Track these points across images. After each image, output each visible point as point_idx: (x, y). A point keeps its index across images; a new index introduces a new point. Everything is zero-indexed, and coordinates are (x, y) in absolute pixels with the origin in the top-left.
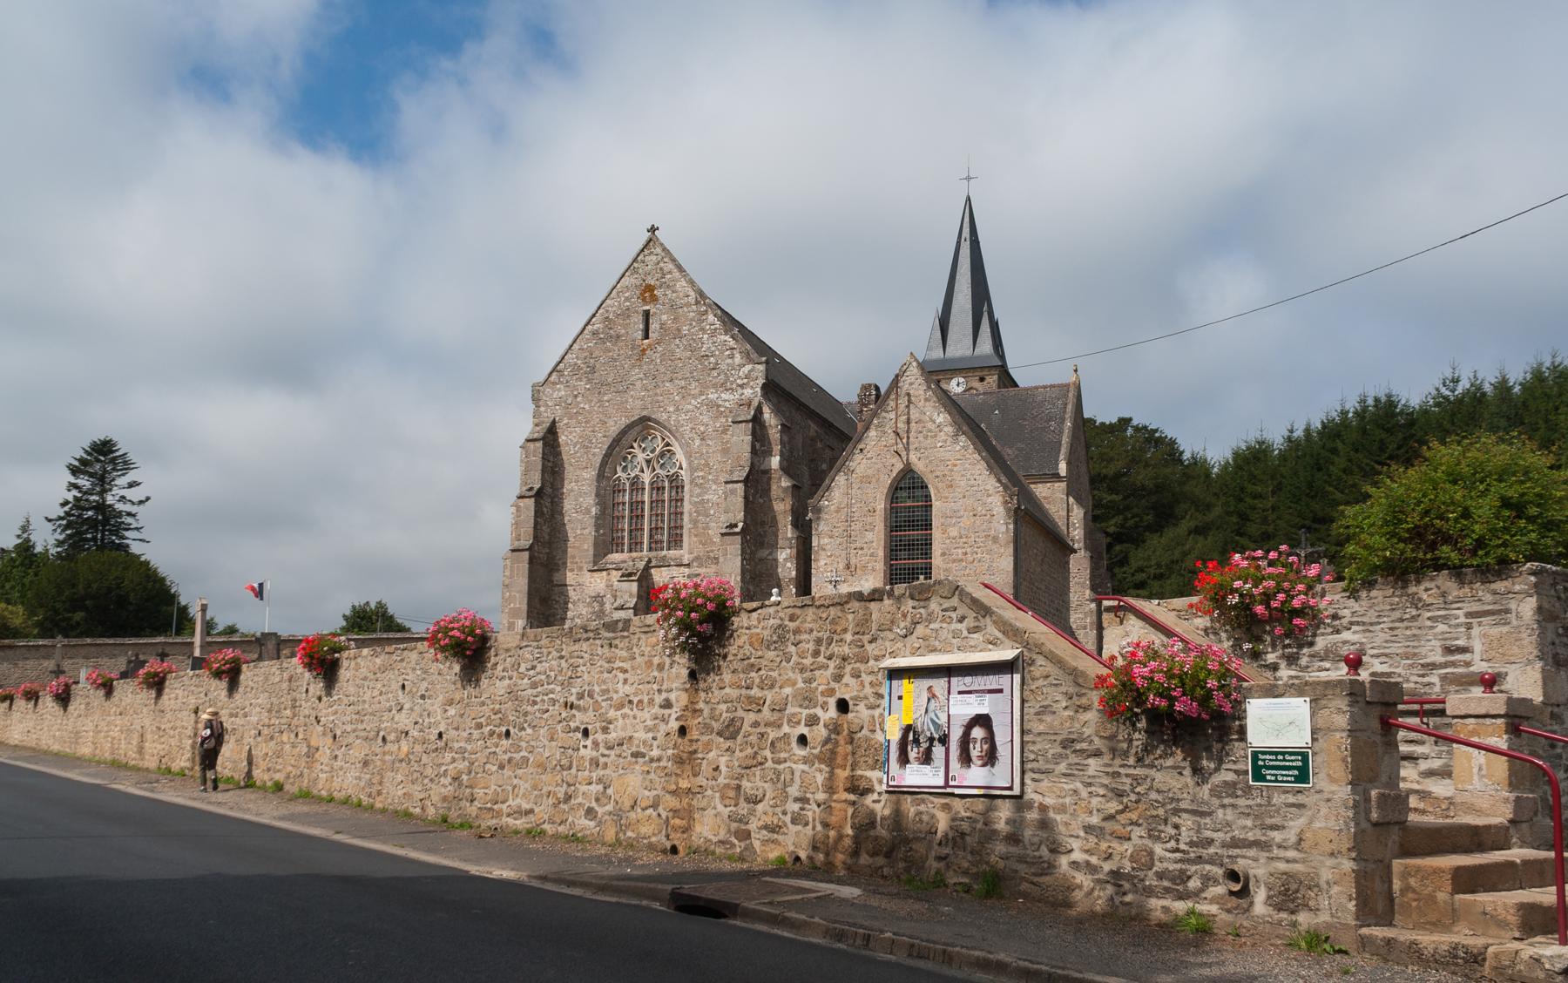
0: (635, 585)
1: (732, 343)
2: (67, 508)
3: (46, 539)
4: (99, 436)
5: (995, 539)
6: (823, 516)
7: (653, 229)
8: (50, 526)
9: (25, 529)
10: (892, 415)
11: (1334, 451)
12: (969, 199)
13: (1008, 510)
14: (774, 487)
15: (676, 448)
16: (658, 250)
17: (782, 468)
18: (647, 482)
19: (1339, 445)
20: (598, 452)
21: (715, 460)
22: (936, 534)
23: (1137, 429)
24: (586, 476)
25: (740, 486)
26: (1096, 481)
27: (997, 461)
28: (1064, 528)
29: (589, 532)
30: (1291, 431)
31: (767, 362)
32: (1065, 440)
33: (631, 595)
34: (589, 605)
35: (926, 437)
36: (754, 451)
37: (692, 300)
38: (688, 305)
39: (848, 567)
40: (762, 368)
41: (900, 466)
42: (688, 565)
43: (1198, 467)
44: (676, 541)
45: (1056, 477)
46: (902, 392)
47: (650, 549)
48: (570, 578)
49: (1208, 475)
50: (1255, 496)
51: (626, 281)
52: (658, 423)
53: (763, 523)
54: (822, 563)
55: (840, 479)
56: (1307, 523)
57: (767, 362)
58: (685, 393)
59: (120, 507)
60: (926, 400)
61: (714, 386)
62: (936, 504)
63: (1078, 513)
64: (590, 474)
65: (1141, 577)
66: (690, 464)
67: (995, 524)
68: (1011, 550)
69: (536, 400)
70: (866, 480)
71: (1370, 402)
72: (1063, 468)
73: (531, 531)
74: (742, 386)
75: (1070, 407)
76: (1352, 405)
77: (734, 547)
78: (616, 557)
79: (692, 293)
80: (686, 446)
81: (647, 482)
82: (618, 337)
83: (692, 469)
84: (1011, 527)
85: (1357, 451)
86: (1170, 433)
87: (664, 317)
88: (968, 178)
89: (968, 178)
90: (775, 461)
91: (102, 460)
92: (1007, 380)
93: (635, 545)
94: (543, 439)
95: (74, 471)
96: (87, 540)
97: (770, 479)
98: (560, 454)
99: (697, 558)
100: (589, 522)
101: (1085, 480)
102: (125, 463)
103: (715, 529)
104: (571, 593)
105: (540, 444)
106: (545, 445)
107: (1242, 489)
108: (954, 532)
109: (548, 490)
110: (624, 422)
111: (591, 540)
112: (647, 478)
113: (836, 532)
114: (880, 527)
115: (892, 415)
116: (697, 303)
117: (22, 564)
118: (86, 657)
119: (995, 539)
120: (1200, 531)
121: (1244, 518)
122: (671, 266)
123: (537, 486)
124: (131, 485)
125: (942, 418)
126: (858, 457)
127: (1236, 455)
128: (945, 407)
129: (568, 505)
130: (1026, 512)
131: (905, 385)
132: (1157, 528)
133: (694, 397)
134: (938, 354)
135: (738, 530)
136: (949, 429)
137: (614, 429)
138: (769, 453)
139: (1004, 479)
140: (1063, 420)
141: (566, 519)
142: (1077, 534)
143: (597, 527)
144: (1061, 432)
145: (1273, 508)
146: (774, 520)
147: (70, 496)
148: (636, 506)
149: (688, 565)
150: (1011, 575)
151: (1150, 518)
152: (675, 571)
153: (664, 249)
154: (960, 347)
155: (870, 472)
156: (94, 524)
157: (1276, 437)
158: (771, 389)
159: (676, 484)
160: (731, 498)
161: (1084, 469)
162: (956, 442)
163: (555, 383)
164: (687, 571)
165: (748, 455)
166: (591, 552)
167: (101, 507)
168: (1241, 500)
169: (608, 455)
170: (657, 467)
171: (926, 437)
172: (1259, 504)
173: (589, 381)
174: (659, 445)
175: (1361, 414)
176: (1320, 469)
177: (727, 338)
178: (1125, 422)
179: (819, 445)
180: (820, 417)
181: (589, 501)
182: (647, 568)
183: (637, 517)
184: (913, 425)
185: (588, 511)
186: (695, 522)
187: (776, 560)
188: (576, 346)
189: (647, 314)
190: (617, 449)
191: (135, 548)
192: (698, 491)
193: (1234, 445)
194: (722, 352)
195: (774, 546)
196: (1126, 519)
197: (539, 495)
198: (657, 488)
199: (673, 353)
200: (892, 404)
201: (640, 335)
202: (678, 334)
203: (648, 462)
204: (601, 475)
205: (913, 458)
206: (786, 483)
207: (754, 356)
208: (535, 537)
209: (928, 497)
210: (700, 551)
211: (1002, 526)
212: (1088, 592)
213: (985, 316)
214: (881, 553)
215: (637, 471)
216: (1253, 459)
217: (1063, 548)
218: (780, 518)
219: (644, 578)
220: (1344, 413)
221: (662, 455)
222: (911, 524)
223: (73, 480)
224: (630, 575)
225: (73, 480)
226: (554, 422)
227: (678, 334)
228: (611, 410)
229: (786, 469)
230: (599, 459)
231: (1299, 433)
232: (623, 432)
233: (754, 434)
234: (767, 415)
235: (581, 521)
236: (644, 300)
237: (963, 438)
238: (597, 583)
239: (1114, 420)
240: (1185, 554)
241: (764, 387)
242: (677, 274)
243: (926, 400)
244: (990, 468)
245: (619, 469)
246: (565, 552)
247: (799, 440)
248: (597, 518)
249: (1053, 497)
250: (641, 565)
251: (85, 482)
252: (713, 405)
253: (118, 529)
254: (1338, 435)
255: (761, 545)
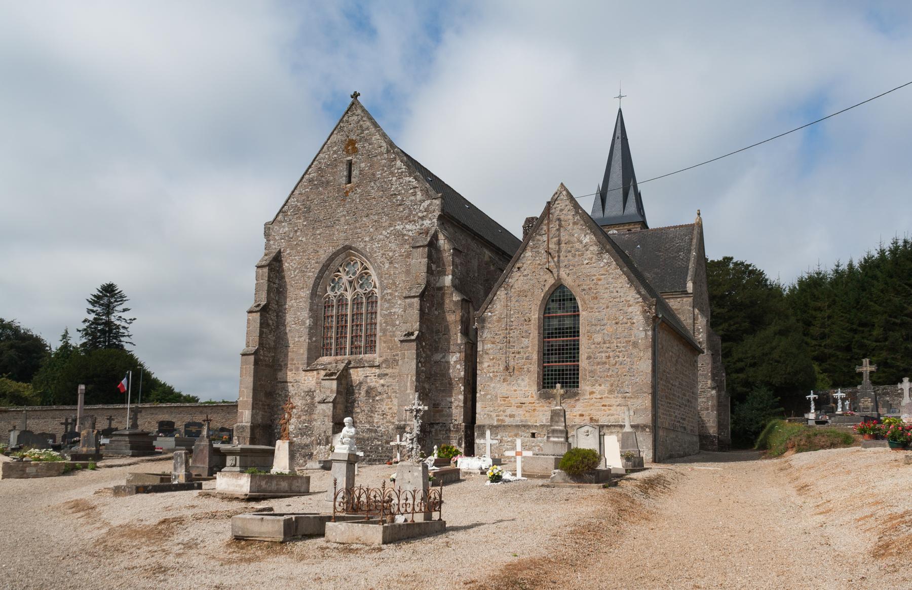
0: (335, 383)
1: (415, 183)
2: (87, 324)
3: (77, 340)
4: (106, 282)
5: (635, 345)
6: (487, 325)
7: (355, 95)
8: (80, 334)
9: (65, 336)
10: (545, 238)
11: (875, 277)
12: (620, 111)
13: (647, 319)
14: (447, 301)
15: (371, 271)
16: (359, 111)
17: (454, 286)
18: (349, 299)
19: (879, 273)
20: (312, 275)
21: (401, 279)
22: (583, 340)
23: (736, 264)
24: (303, 294)
25: (417, 300)
26: (712, 298)
27: (636, 274)
28: (692, 332)
29: (305, 339)
30: (838, 266)
31: (442, 197)
32: (691, 265)
33: (332, 391)
34: (304, 398)
35: (574, 256)
36: (429, 271)
37: (384, 150)
38: (381, 154)
39: (507, 368)
40: (438, 202)
41: (551, 281)
42: (378, 366)
43: (774, 292)
44: (371, 347)
45: (685, 292)
46: (553, 217)
47: (352, 353)
48: (290, 376)
49: (781, 295)
50: (816, 309)
51: (335, 138)
52: (357, 250)
53: (438, 332)
54: (486, 365)
55: (501, 293)
56: (855, 327)
57: (442, 197)
58: (378, 226)
59: (118, 323)
60: (574, 223)
61: (401, 219)
62: (583, 314)
63: (702, 322)
64: (305, 293)
65: (740, 365)
66: (381, 283)
67: (635, 331)
68: (649, 354)
69: (267, 235)
70: (523, 293)
71: (901, 243)
72: (690, 286)
73: (257, 339)
74: (422, 218)
75: (695, 241)
76: (887, 245)
77: (409, 355)
78: (325, 359)
79: (384, 144)
80: (378, 268)
81: (349, 299)
82: (328, 182)
83: (383, 288)
84: (650, 333)
85: (891, 277)
86: (759, 267)
87: (363, 165)
88: (620, 97)
89: (620, 97)
90: (448, 280)
91: (108, 296)
92: (644, 225)
93: (340, 350)
94: (269, 265)
95: (93, 303)
96: (100, 342)
97: (444, 294)
98: (283, 277)
99: (386, 361)
100: (305, 331)
101: (706, 296)
102: (121, 297)
103: (399, 335)
104: (290, 388)
105: (266, 270)
106: (270, 270)
107: (806, 305)
108: (598, 338)
109: (274, 306)
110: (331, 250)
111: (306, 346)
112: (349, 296)
113: (498, 339)
114: (534, 333)
115: (545, 238)
116: (388, 152)
117: (63, 356)
118: (53, 418)
119: (635, 345)
120: (783, 333)
121: (808, 324)
122: (368, 123)
123: (263, 303)
124: (125, 310)
125: (588, 238)
126: (516, 274)
127: (801, 282)
128: (590, 228)
129: (289, 318)
130: (664, 321)
131: (556, 212)
132: (752, 331)
133: (385, 229)
134: (599, 215)
135: (413, 337)
136: (594, 249)
137: (323, 257)
138: (443, 273)
139: (643, 291)
140: (689, 251)
141: (288, 329)
142: (701, 337)
143: (311, 336)
144: (688, 260)
145: (829, 317)
146: (447, 330)
147: (92, 317)
148: (341, 317)
149: (378, 366)
150: (650, 376)
151: (746, 325)
152: (368, 371)
153: (364, 110)
154: (614, 208)
155: (526, 287)
156: (104, 333)
157: (828, 268)
158: (445, 219)
159: (371, 299)
160: (409, 311)
161: (705, 288)
162: (600, 259)
163: (281, 222)
164: (377, 371)
165: (424, 275)
166: (306, 356)
167: (109, 323)
168: (805, 312)
169: (319, 277)
170: (357, 286)
171: (574, 256)
172: (819, 315)
173: (306, 219)
174: (359, 268)
175: (894, 251)
176: (864, 290)
177: (411, 179)
178: (728, 260)
179: (492, 268)
180: (494, 246)
181: (305, 315)
182: (347, 369)
183: (341, 328)
184: (563, 245)
185: (304, 323)
186: (384, 331)
187: (448, 362)
188: (297, 192)
189: (350, 164)
190: (326, 273)
191: (127, 347)
192: (386, 305)
193: (799, 275)
194: (407, 191)
195: (447, 351)
196: (730, 325)
197: (264, 310)
198: (357, 302)
199: (368, 193)
200: (545, 228)
201: (344, 180)
202: (373, 178)
203: (351, 282)
204: (314, 294)
205: (563, 274)
206: (456, 297)
207: (432, 193)
208: (261, 344)
209: (576, 308)
210: (388, 355)
211: (641, 332)
212: (709, 382)
213: (632, 189)
214: (535, 357)
215: (342, 291)
216: (812, 285)
217: (694, 349)
218: (452, 327)
219: (343, 378)
220: (882, 252)
221: (361, 277)
222: (561, 332)
223: (91, 307)
224: (332, 374)
225: (91, 307)
226: (280, 252)
227: (373, 178)
228: (322, 241)
229: (459, 286)
230: (311, 282)
231: (844, 267)
232: (331, 259)
233: (430, 256)
234: (442, 242)
235: (298, 331)
236: (348, 152)
237: (606, 256)
238: (309, 380)
239: (720, 259)
240: (773, 349)
241: (440, 218)
242: (373, 130)
243: (574, 223)
244: (630, 281)
245: (329, 289)
246: (286, 355)
247: (475, 263)
248: (310, 328)
249: (685, 309)
250: (341, 366)
251: (98, 309)
252: (399, 235)
253: (118, 336)
254: (878, 266)
255: (437, 350)
